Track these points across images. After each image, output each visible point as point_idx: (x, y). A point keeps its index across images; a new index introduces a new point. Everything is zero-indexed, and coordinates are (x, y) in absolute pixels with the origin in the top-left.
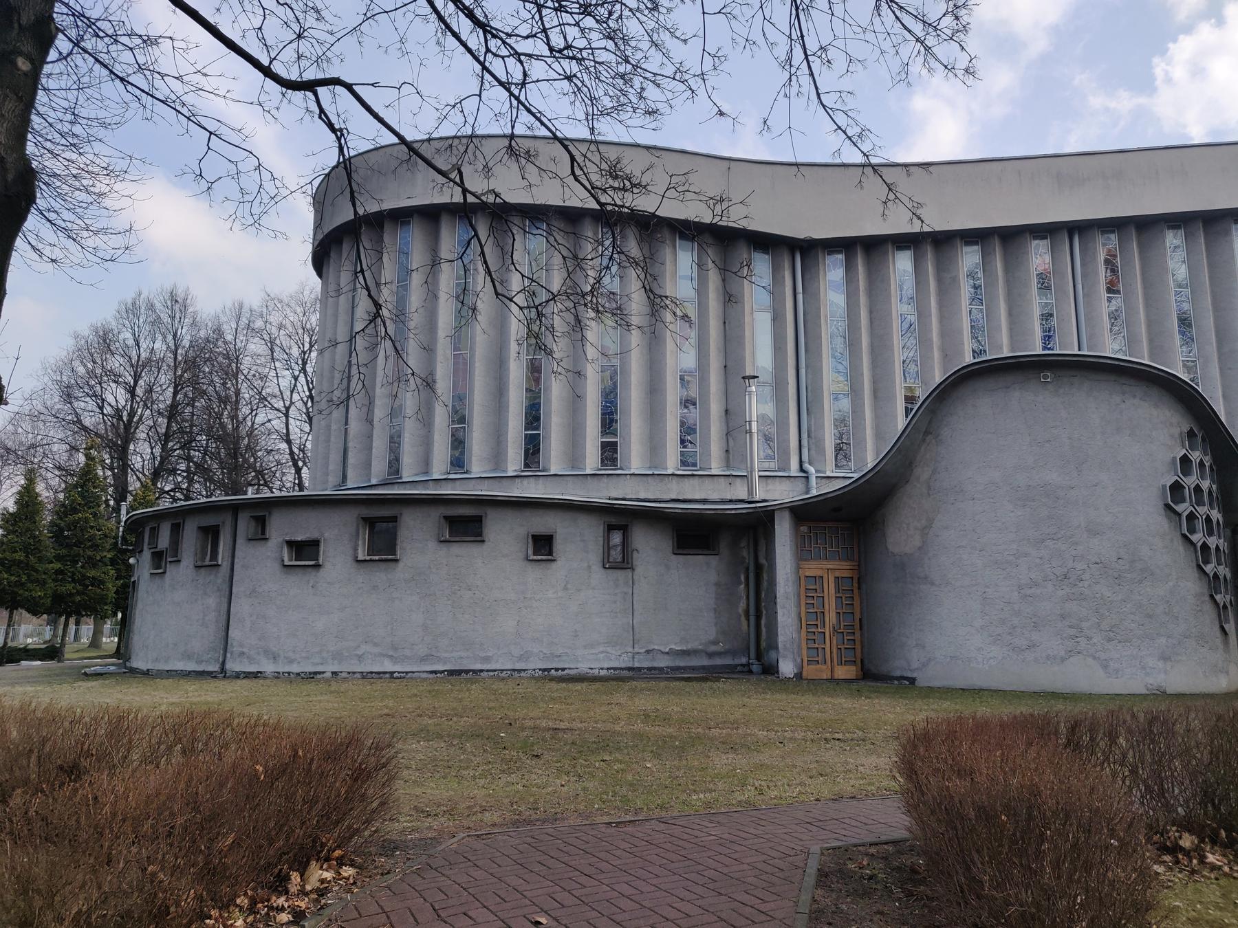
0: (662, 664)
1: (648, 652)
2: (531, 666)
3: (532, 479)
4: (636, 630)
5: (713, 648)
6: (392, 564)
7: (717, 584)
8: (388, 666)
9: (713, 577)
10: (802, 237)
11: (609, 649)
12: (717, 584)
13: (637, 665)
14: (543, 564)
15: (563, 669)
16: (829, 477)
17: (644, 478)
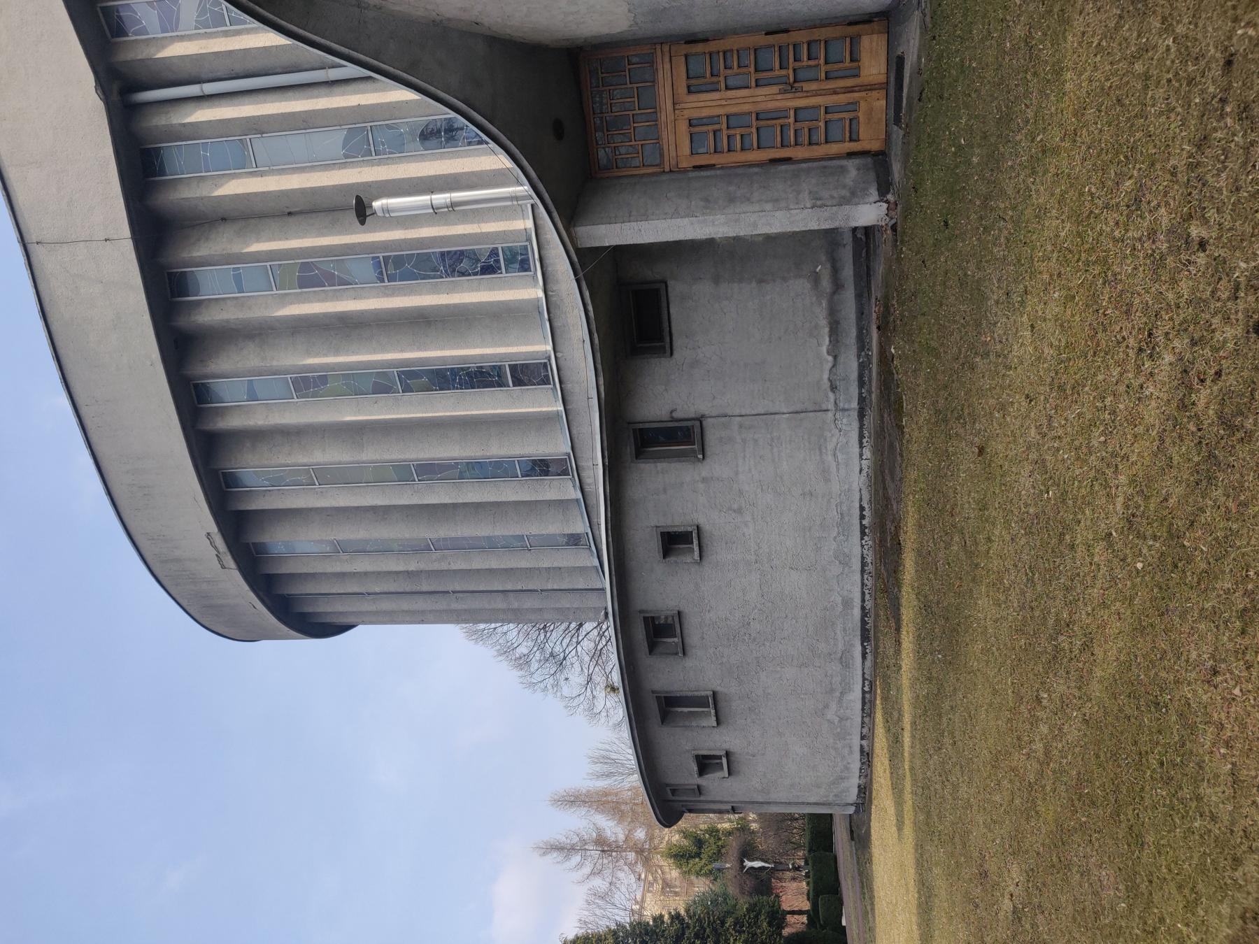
0: (854, 366)
1: (833, 388)
2: (857, 551)
3: (583, 474)
4: (799, 407)
5: (826, 283)
6: (719, 697)
7: (717, 280)
8: (856, 695)
9: (704, 289)
10: (99, 105)
11: (831, 446)
12: (717, 280)
13: (855, 405)
14: (705, 541)
15: (862, 509)
16: (486, 188)
17: (558, 332)
